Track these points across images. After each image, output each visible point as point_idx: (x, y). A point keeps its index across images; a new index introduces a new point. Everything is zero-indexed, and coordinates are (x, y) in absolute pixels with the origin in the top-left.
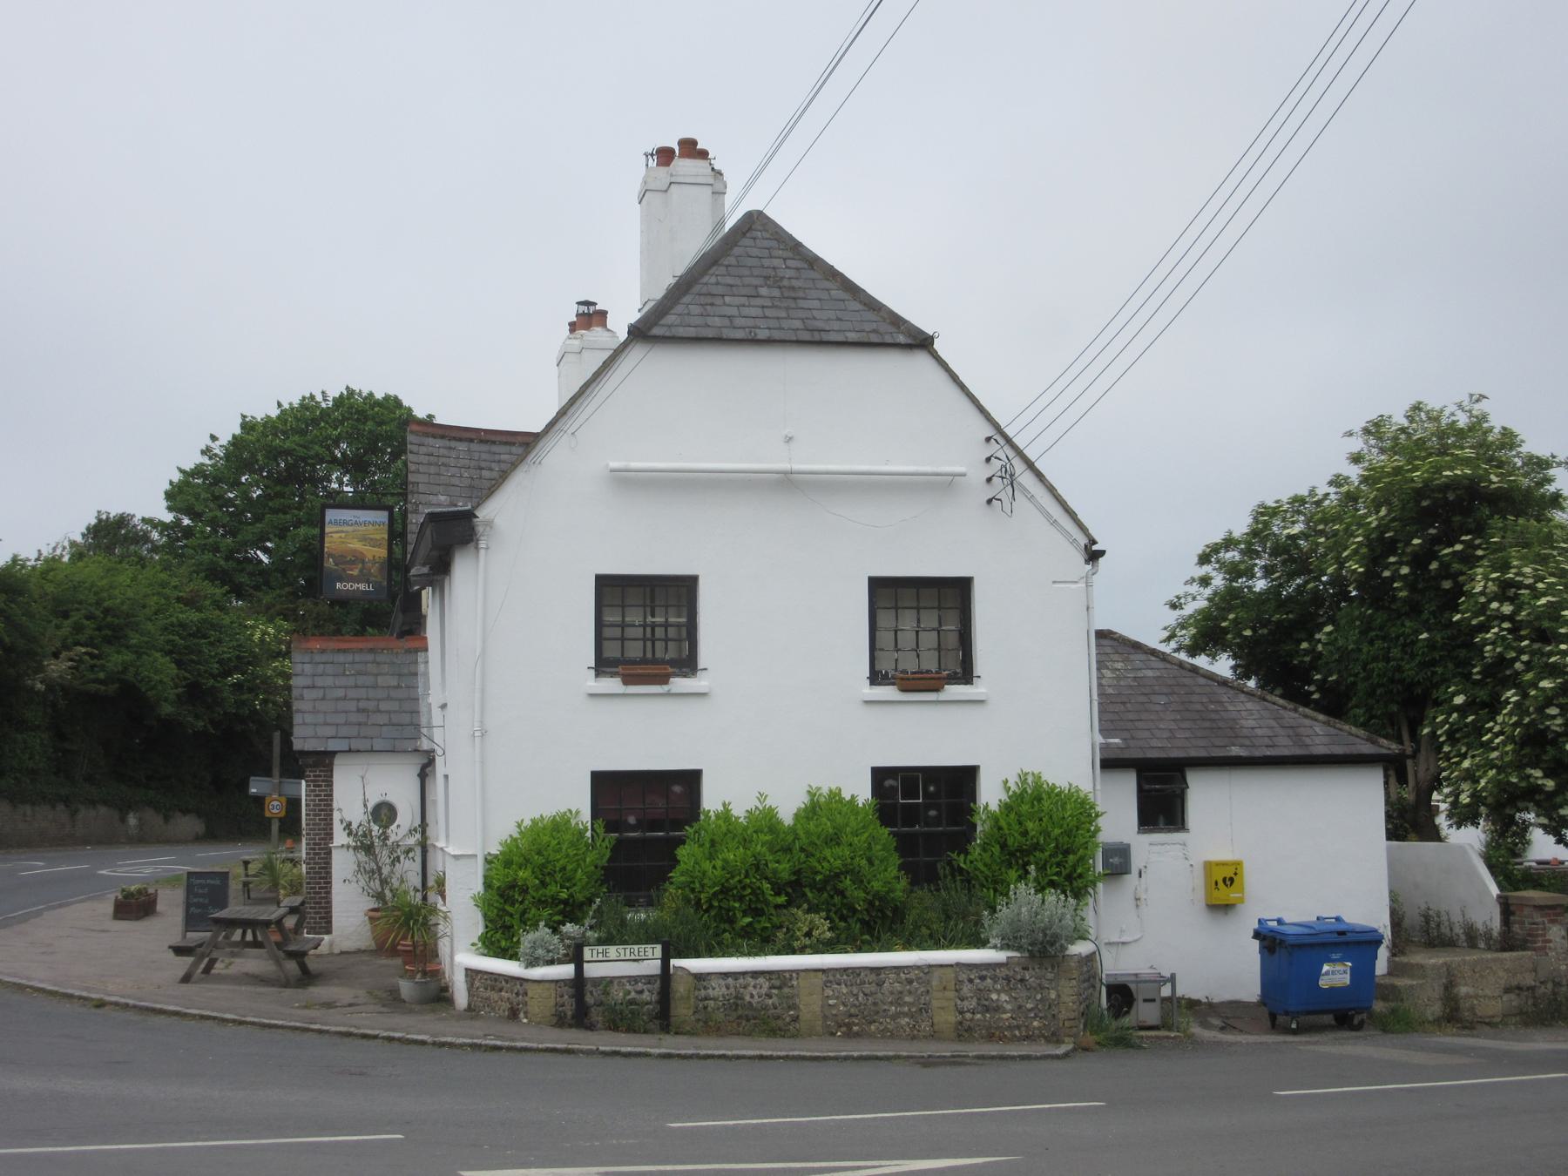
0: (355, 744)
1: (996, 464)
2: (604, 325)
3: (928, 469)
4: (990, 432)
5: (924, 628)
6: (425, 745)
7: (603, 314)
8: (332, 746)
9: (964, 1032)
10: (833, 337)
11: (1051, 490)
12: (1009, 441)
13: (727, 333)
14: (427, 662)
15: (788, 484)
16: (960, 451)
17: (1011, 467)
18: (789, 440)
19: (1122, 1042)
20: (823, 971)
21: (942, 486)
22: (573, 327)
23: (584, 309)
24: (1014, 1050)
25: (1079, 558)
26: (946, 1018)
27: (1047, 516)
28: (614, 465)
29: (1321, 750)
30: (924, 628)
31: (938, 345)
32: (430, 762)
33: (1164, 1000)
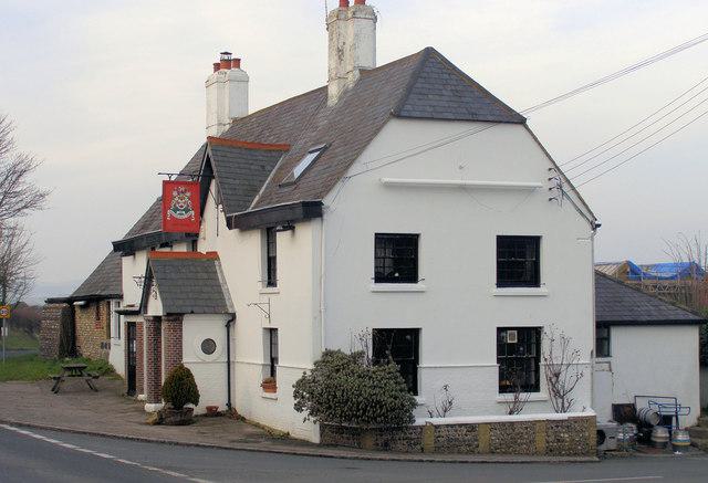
0: (206, 309)
1: (555, 182)
2: (238, 66)
3: (505, 183)
4: (552, 166)
5: (518, 262)
6: (230, 311)
7: (237, 61)
8: (184, 310)
9: (550, 451)
10: (481, 118)
11: (577, 193)
12: (559, 170)
13: (435, 115)
14: (220, 266)
15: (463, 188)
16: (537, 177)
17: (562, 187)
18: (461, 168)
19: (604, 456)
20: (490, 424)
21: (530, 191)
22: (217, 67)
23: (226, 57)
24: (578, 459)
25: (589, 227)
26: (541, 444)
27: (575, 205)
28: (387, 180)
29: (672, 318)
30: (518, 262)
31: (528, 123)
32: (233, 317)
33: (619, 440)
